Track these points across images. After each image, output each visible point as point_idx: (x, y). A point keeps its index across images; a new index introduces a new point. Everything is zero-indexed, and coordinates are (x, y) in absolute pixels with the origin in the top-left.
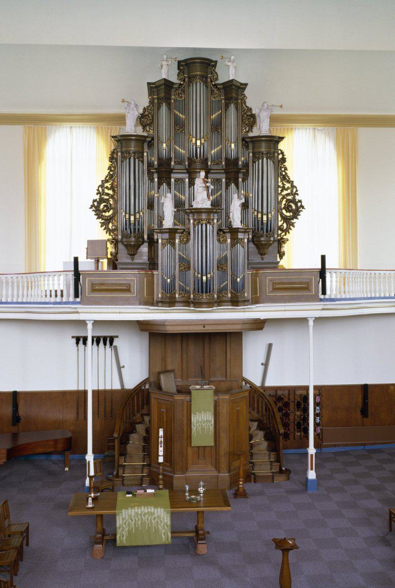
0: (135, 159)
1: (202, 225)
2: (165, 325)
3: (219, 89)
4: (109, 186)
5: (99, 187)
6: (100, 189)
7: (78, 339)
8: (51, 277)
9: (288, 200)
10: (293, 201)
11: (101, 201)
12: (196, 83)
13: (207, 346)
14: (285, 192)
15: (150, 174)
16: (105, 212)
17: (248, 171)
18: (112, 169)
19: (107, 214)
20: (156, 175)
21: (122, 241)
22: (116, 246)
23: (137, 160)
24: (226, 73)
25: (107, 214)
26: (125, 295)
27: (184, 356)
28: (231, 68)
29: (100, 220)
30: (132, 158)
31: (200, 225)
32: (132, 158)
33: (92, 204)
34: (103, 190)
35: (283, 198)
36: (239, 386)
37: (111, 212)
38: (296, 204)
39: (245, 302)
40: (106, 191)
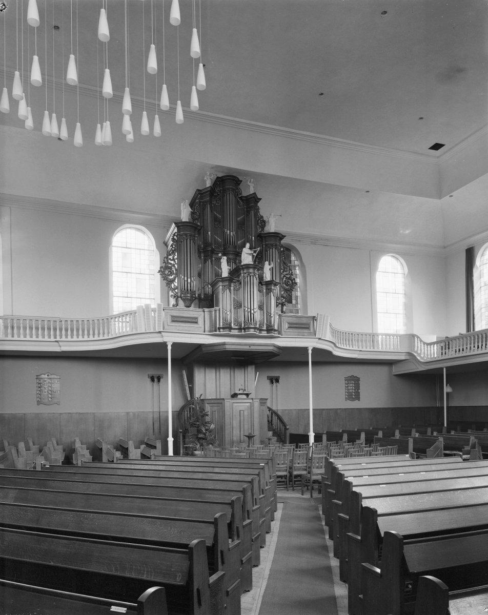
0: (190, 240)
1: (250, 276)
2: (482, 256)
3: (242, 200)
4: (172, 258)
5: (164, 258)
6: (165, 259)
7: (152, 379)
8: (128, 316)
9: (286, 278)
10: (290, 278)
11: (167, 268)
12: (229, 194)
13: (232, 374)
14: (285, 273)
15: (199, 253)
16: (169, 275)
17: (262, 257)
18: (174, 246)
19: (171, 277)
20: (202, 255)
21: (181, 297)
22: (177, 301)
23: (192, 241)
24: (249, 189)
25: (171, 277)
26: (15, 558)
27: (246, 376)
28: (251, 187)
29: (165, 281)
30: (188, 240)
31: (249, 277)
32: (188, 240)
33: (159, 269)
34: (168, 261)
35: (284, 276)
36: (159, 381)
37: (173, 277)
38: (292, 281)
39: (309, 326)
40: (170, 261)
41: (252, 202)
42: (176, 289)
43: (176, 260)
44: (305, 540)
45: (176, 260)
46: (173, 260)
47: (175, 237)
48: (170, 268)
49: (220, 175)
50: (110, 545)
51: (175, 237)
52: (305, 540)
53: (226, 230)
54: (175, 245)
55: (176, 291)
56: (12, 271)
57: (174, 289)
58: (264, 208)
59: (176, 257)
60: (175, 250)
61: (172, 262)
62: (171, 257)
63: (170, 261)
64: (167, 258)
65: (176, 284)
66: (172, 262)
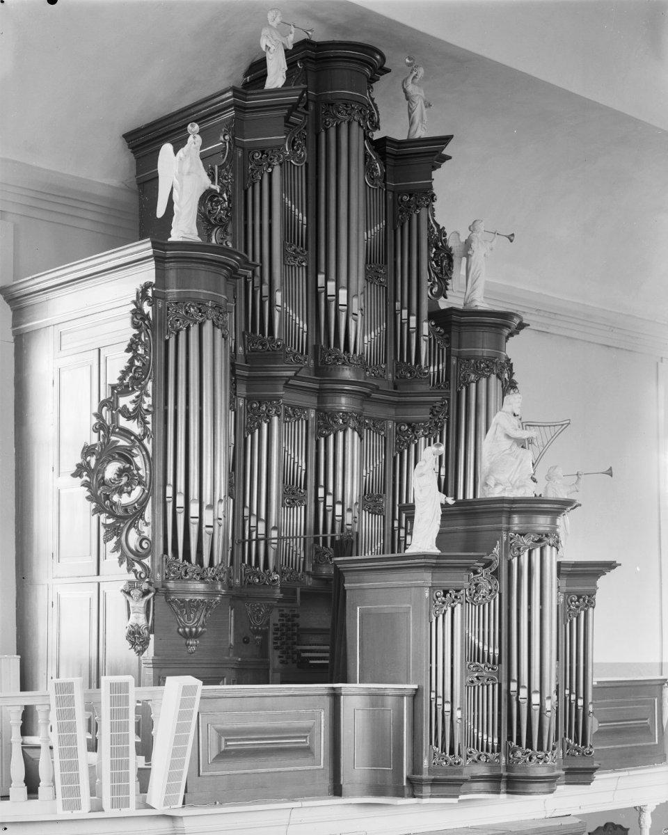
3: (383, 156)
4: (131, 407)
6: (106, 414)
11: (106, 452)
18: (141, 351)
19: (125, 499)
25: (125, 499)
33: (445, 230)
34: (114, 419)
40: (123, 422)
41: (407, 170)
42: (145, 556)
43: (149, 418)
44: (171, 829)
45: (149, 418)
46: (137, 415)
47: (147, 309)
48: (126, 456)
49: (319, 36)
50: (16, 378)
51: (147, 309)
52: (171, 829)
53: (331, 286)
54: (145, 345)
55: (147, 561)
56: (659, 500)
57: (139, 555)
58: (454, 200)
59: (148, 401)
60: (145, 369)
61: (134, 427)
62: (126, 401)
63: (123, 422)
64: (109, 403)
65: (147, 531)
66: (134, 427)
